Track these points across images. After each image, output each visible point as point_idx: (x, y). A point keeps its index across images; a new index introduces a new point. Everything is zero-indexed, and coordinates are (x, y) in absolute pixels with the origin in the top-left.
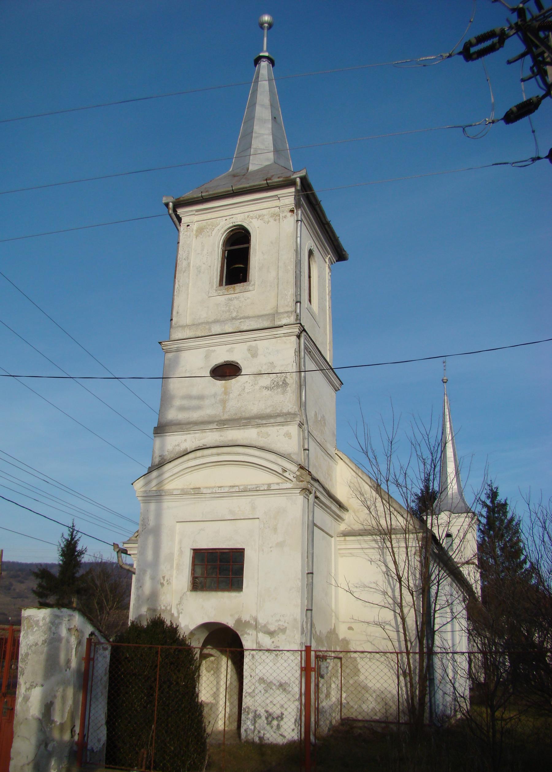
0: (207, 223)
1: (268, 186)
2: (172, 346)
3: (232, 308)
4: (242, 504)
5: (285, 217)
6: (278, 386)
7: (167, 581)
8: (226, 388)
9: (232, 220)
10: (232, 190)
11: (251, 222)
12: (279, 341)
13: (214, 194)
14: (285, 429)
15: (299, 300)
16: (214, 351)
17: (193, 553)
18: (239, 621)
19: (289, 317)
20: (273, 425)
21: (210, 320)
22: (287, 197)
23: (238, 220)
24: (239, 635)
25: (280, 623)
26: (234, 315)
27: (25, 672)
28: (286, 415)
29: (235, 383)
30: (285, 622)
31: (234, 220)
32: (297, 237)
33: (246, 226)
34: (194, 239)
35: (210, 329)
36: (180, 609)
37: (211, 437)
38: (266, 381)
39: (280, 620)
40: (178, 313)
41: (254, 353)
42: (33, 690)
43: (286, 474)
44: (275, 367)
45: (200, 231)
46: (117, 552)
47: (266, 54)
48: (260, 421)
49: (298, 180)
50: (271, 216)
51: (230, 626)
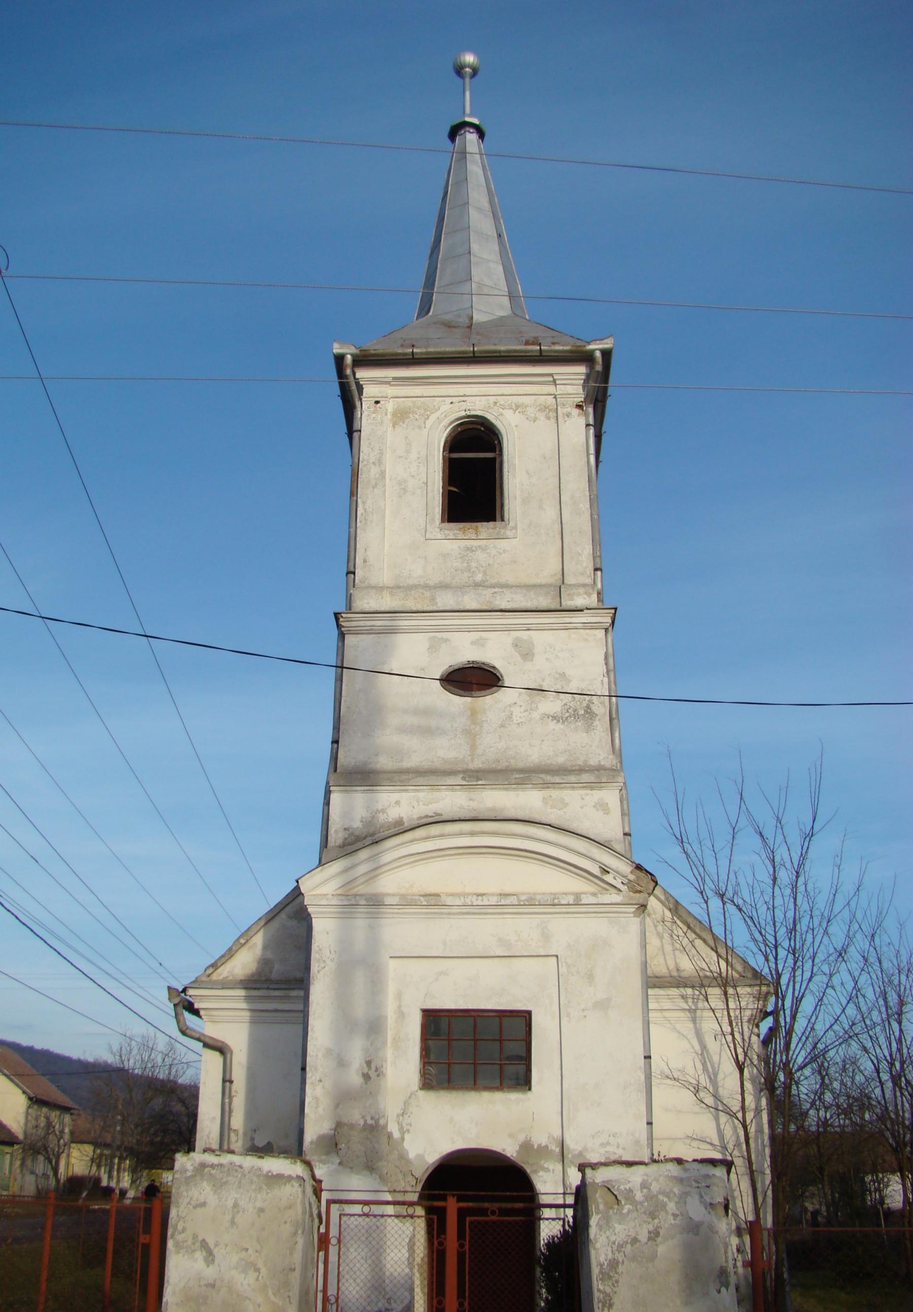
0: (414, 402)
1: (541, 355)
2: (362, 623)
3: (473, 565)
4: (522, 928)
6: (575, 715)
7: (377, 1070)
8: (473, 713)
9: (464, 406)
11: (502, 415)
12: (573, 636)
13: (438, 353)
15: (598, 566)
16: (446, 640)
18: (526, 1146)
19: (589, 595)
20: (573, 786)
21: (431, 583)
22: (572, 380)
23: (477, 408)
24: (528, 1171)
25: (608, 1148)
26: (479, 577)
27: (615, 1300)
29: (491, 703)
30: (618, 1146)
31: (467, 405)
32: (588, 454)
33: (493, 420)
34: (390, 429)
35: (433, 599)
36: (404, 1125)
37: (451, 800)
38: (551, 705)
39: (608, 1143)
40: (365, 561)
41: (527, 654)
43: (609, 878)
44: (569, 681)
45: (400, 416)
46: (175, 1005)
47: (475, 121)
48: (549, 778)
49: (598, 354)
50: (540, 410)
51: (509, 1155)
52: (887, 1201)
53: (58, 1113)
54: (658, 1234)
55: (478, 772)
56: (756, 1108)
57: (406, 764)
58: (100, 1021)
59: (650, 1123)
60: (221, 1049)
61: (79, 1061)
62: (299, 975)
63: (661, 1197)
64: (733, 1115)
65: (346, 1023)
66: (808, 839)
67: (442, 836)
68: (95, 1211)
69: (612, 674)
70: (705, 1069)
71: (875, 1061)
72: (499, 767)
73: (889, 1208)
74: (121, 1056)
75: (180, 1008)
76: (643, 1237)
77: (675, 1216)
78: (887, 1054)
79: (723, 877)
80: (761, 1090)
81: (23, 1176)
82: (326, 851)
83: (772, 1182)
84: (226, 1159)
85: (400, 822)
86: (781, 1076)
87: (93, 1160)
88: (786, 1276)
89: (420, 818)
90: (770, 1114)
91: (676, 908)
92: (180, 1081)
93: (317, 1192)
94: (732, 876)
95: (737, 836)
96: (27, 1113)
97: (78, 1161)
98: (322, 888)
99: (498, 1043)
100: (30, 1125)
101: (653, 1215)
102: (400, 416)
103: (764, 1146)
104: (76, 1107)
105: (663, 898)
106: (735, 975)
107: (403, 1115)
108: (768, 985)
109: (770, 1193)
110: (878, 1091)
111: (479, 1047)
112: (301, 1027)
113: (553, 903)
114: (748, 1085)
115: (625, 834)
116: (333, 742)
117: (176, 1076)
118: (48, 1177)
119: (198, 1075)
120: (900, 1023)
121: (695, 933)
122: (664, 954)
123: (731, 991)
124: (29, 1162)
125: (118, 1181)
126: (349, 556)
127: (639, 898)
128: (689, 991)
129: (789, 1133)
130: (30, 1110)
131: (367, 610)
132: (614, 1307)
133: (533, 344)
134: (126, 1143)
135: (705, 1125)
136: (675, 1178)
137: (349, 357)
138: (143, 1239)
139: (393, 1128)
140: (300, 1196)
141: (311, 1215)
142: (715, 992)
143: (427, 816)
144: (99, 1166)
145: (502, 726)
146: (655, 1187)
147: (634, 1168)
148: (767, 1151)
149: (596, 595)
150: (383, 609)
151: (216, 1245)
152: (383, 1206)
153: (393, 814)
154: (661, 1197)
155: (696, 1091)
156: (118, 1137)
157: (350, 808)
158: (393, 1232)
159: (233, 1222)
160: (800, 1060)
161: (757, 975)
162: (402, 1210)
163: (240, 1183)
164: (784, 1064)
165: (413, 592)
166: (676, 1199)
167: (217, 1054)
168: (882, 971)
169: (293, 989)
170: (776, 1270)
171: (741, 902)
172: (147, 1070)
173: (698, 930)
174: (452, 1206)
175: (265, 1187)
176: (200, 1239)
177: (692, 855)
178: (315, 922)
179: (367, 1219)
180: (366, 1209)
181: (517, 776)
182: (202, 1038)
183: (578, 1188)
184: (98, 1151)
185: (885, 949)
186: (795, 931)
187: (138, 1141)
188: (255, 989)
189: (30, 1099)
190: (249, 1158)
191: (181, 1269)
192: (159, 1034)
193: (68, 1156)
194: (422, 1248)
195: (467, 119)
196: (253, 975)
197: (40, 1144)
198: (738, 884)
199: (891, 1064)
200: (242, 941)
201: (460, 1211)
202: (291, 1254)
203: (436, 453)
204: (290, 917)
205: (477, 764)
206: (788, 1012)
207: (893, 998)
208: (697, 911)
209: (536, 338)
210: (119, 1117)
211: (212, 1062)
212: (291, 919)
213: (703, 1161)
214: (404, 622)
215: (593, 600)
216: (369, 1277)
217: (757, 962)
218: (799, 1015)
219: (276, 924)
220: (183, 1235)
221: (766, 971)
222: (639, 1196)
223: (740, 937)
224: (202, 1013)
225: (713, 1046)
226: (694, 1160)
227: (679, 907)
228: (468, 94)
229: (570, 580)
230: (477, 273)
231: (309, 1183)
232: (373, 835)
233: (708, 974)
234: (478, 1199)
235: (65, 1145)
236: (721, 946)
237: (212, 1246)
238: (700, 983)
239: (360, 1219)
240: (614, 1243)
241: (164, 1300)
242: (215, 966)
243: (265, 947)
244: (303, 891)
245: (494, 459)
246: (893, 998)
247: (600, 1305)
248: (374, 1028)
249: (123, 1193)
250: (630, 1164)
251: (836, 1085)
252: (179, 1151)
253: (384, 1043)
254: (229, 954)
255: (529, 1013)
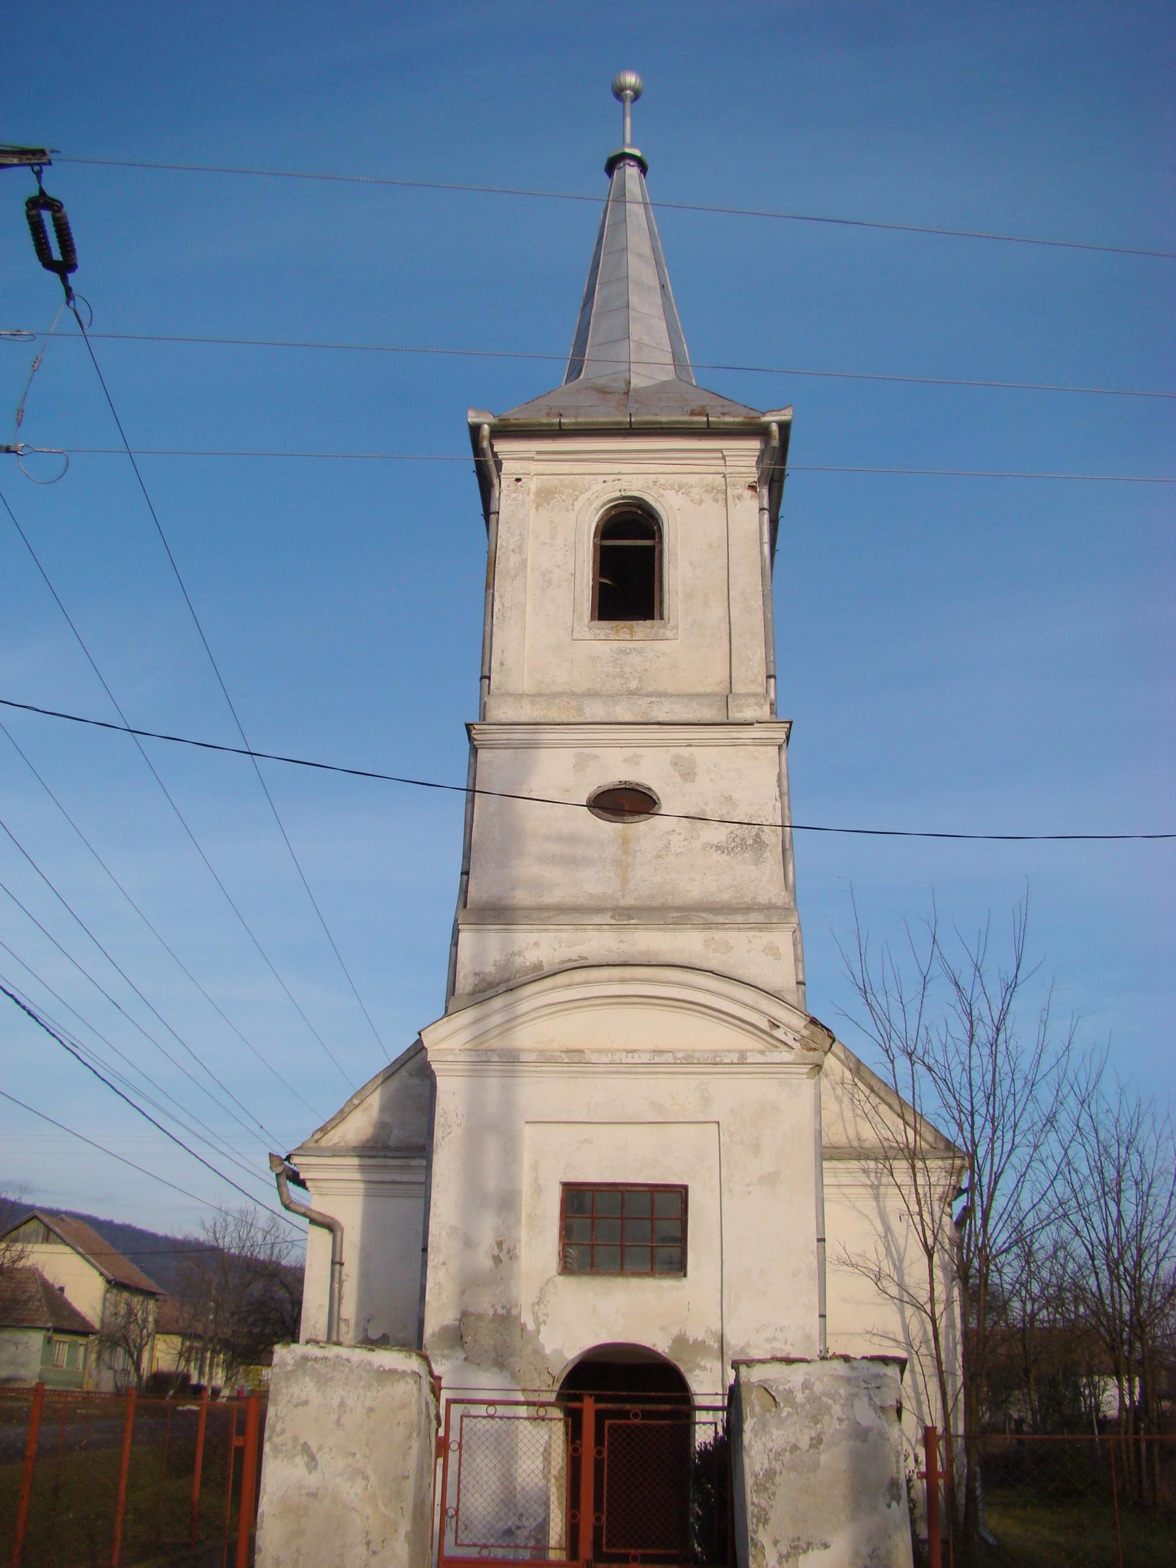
1: (708, 427)
2: (497, 736)
3: (627, 670)
4: (679, 1091)
5: (739, 497)
6: (743, 845)
7: (509, 1251)
8: (625, 841)
9: (619, 485)
10: (631, 423)
11: (663, 496)
13: (593, 424)
14: (764, 938)
17: (563, 1191)
18: (680, 1341)
19: (761, 706)
21: (578, 690)
23: (633, 488)
25: (775, 1344)
26: (633, 685)
27: (771, 1514)
28: (768, 909)
29: (643, 829)
30: (786, 1342)
31: (623, 485)
32: (761, 544)
34: (533, 511)
35: (580, 709)
36: (540, 1314)
37: (598, 941)
38: (716, 834)
40: (502, 664)
41: (688, 773)
42: (801, 1558)
43: (778, 1033)
45: (545, 496)
46: (277, 1175)
47: (637, 153)
48: (710, 917)
50: (707, 491)
51: (660, 1351)
52: (1104, 1408)
53: (141, 1298)
54: (820, 1441)
55: (629, 909)
56: (947, 1299)
57: (549, 899)
58: (191, 1195)
59: (823, 1316)
60: (330, 1226)
61: (166, 1239)
62: (421, 1141)
63: (824, 1399)
64: (919, 1307)
65: (475, 1197)
66: (1010, 990)
67: (586, 983)
68: (183, 1413)
69: (786, 799)
70: (889, 1253)
71: (1090, 1247)
72: (654, 904)
73: (1105, 1416)
74: (215, 1233)
75: (283, 1179)
76: (804, 1443)
77: (840, 1420)
78: (1102, 1237)
79: (912, 1033)
80: (953, 1279)
81: (99, 1371)
82: (453, 999)
83: (964, 1384)
84: (333, 1351)
85: (539, 966)
86: (976, 1263)
87: (181, 1354)
88: (978, 1492)
89: (563, 962)
90: (964, 1307)
91: (858, 1068)
92: (283, 1262)
93: (436, 1390)
94: (922, 1032)
95: (928, 986)
96: (105, 1299)
97: (163, 1354)
98: (448, 1042)
99: (647, 1223)
100: (108, 1312)
101: (815, 1420)
102: (545, 496)
103: (955, 1344)
104: (162, 1291)
105: (842, 1056)
106: (925, 1146)
107: (538, 1303)
108: (963, 1158)
109: (961, 1397)
110: (1092, 1281)
111: (626, 1227)
112: (422, 1201)
113: (714, 1062)
114: (938, 1273)
115: (798, 983)
116: (462, 873)
117: (279, 1256)
118: (129, 1373)
119: (304, 1255)
120: (1118, 1204)
121: (880, 1097)
122: (843, 1121)
123: (919, 1164)
124: (106, 1356)
125: (211, 1378)
126: (483, 658)
127: (814, 1056)
128: (872, 1164)
129: (984, 1329)
130: (108, 1295)
131: (504, 721)
132: (771, 1522)
133: (699, 414)
134: (220, 1335)
135: (888, 1318)
136: (841, 1377)
137: (486, 426)
138: (237, 1442)
139: (527, 1319)
140: (416, 1394)
141: (428, 1416)
142: (901, 1165)
143: (570, 960)
144: (188, 1361)
145: (658, 857)
146: (818, 1388)
147: (795, 1366)
148: (960, 1349)
149: (768, 707)
150: (522, 720)
151: (320, 1448)
152: (514, 1407)
153: (531, 957)
154: (824, 1399)
155: (878, 1278)
156: (211, 1326)
157: (481, 949)
158: (525, 1441)
159: (338, 1423)
160: (1000, 1241)
161: (949, 1146)
162: (532, 1411)
163: (347, 1378)
164: (980, 1250)
165: (557, 701)
166: (842, 1401)
167: (326, 1231)
168: (1098, 1142)
169: (414, 1158)
170: (967, 1486)
171: (931, 1062)
172: (246, 1249)
173: (882, 1094)
174: (589, 1407)
175: (375, 1383)
176: (301, 1441)
177: (876, 1007)
178: (440, 1081)
179: (492, 1422)
180: (491, 1410)
181: (675, 915)
182: (309, 1213)
183: (731, 1388)
184: (188, 1343)
185: (1102, 1117)
186: (994, 1095)
187: (234, 1331)
188: (370, 1157)
189: (109, 1282)
190: (357, 1350)
191: (279, 1476)
192: (259, 1207)
193: (152, 1348)
194: (559, 1459)
195: (628, 150)
196: (368, 1141)
197: (119, 1334)
198: (929, 1041)
199: (1108, 1249)
200: (356, 1102)
201: (600, 1416)
202: (405, 1459)
203: (586, 540)
204: (411, 1075)
205: (629, 901)
206: (985, 1189)
207: (1110, 1173)
208: (883, 1072)
209: (703, 407)
210: (212, 1304)
211: (321, 1237)
212: (413, 1075)
213: (873, 1359)
214: (547, 736)
215: (765, 712)
216: (498, 1491)
217: (950, 1131)
218: (997, 1193)
219: (395, 1082)
220: (282, 1438)
221: (959, 1142)
222: (800, 1397)
223: (931, 1103)
224: (309, 1184)
225: (899, 1228)
226: (864, 1358)
227: (862, 1068)
228: (628, 120)
229: (738, 688)
230: (635, 330)
231: (426, 1380)
232: (508, 980)
233: (894, 1144)
234: (626, 1404)
235: (149, 1336)
236: (909, 1112)
237: (314, 1450)
238: (884, 1155)
239: (484, 1421)
240: (771, 1450)
241: (260, 1510)
242: (324, 1130)
243: (383, 1109)
244: (426, 1045)
245: (652, 548)
246: (1110, 1173)
247: (755, 1520)
248: (507, 1203)
249: (216, 1392)
250: (789, 1361)
251: (1045, 1274)
252: (278, 1343)
253: (518, 1220)
254: (341, 1116)
255: (685, 1188)
